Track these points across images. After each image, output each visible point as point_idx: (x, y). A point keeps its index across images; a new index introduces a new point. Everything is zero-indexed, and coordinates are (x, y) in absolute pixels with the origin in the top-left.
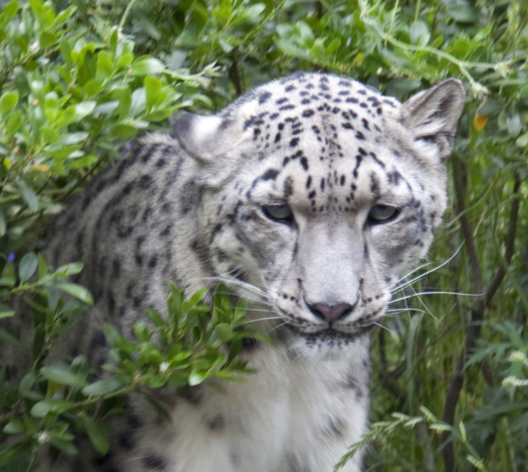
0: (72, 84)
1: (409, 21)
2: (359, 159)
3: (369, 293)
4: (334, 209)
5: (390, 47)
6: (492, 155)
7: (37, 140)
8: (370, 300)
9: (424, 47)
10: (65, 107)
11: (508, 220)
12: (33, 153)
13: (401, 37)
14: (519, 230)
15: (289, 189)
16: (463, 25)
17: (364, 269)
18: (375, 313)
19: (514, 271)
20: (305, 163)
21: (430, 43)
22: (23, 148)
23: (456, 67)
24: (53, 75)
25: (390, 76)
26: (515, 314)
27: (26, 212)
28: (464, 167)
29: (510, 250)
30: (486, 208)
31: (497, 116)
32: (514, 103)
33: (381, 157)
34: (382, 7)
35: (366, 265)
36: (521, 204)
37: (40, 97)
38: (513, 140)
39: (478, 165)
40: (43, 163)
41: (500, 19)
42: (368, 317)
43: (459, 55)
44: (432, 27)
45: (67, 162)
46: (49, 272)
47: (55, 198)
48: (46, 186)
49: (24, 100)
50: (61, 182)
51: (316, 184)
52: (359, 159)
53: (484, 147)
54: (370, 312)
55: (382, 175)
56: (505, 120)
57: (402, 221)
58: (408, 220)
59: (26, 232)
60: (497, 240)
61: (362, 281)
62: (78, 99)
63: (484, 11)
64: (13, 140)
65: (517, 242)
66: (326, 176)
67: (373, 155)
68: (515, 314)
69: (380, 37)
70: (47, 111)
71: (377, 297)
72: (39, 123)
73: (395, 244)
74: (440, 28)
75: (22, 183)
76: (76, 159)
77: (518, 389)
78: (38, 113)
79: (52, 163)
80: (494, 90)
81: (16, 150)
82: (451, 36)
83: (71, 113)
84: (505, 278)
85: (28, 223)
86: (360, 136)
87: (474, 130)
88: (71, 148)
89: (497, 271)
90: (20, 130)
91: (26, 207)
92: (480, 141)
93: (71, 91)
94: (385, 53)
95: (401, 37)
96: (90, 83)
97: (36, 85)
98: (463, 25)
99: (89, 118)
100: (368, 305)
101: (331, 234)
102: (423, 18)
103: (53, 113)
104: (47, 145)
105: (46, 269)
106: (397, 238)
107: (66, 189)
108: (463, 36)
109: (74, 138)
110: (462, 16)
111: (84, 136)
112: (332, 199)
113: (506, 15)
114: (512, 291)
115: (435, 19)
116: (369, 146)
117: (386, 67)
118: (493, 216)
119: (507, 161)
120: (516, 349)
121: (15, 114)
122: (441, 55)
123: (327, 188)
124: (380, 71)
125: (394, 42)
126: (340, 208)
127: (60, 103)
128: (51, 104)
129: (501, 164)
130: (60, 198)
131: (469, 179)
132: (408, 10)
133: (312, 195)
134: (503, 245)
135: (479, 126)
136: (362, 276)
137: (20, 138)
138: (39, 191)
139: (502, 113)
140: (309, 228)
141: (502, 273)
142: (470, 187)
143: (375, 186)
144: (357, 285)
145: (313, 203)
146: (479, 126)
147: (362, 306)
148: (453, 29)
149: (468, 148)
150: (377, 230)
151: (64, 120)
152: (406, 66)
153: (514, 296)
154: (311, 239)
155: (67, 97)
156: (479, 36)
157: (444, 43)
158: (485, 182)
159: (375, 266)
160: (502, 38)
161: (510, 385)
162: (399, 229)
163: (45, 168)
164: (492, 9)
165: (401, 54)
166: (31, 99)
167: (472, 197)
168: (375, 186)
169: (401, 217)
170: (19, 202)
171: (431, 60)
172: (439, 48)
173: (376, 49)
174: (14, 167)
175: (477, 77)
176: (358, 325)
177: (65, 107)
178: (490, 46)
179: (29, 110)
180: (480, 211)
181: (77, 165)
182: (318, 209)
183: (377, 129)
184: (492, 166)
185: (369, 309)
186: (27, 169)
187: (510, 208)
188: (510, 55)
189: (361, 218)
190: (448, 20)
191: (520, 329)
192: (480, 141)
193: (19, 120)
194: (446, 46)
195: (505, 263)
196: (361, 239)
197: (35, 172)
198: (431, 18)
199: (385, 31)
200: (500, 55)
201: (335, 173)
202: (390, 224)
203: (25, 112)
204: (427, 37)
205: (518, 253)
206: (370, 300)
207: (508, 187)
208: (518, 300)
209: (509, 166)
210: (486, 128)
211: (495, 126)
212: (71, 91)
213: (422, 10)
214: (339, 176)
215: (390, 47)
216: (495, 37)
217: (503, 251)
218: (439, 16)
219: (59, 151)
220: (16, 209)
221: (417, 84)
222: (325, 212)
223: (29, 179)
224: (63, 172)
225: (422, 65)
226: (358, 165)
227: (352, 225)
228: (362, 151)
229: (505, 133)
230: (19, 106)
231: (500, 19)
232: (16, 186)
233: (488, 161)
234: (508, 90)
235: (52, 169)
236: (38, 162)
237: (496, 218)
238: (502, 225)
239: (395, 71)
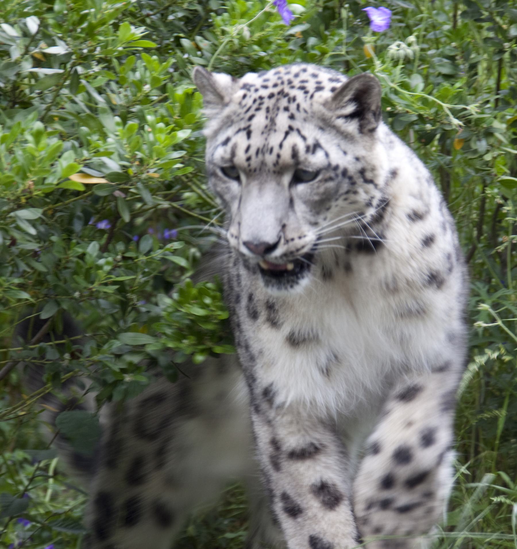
0: (176, 117)
1: (409, 75)
2: (287, 134)
3: (290, 234)
4: (265, 171)
5: (396, 92)
6: (466, 167)
7: (151, 157)
8: (293, 240)
9: (419, 93)
10: (170, 133)
11: (478, 212)
12: (148, 165)
13: (404, 85)
14: (486, 219)
15: (233, 154)
16: (447, 77)
17: (287, 216)
18: (298, 250)
19: (482, 247)
20: (249, 134)
21: (423, 91)
22: (141, 161)
23: (441, 106)
24: (162, 111)
25: (396, 112)
26: (483, 278)
27: (146, 207)
28: (448, 175)
29: (480, 233)
30: (463, 203)
31: (470, 140)
32: (483, 130)
33: (305, 132)
34: (391, 64)
35: (291, 213)
36: (488, 201)
37: (153, 126)
38: (481, 156)
39: (457, 174)
40: (155, 172)
41: (473, 72)
42: (292, 253)
43: (442, 98)
44: (426, 78)
45: (172, 171)
46: (161, 248)
47: (166, 197)
48: (159, 189)
49: (142, 128)
50: (169, 186)
51: (253, 151)
52: (287, 134)
53: (462, 161)
54: (293, 249)
55: (301, 146)
56: (475, 143)
57: (320, 181)
58: (326, 180)
59: (146, 220)
60: (471, 225)
61: (284, 226)
62: (180, 127)
63: (462, 67)
64: (134, 156)
65: (485, 227)
66: (261, 147)
67: (299, 131)
68: (483, 278)
69: (389, 85)
70: (158, 135)
71: (300, 238)
72: (152, 144)
73: (316, 198)
74: (432, 79)
75: (140, 185)
76: (179, 169)
77: (486, 329)
78: (151, 137)
79: (162, 172)
80: (468, 122)
81: (137, 163)
82: (438, 84)
83: (174, 137)
84: (476, 252)
85: (147, 215)
86: (292, 117)
87: (455, 150)
88: (174, 161)
89: (470, 247)
90: (139, 150)
91: (145, 204)
92: (459, 157)
93: (175, 123)
94: (393, 97)
95: (404, 85)
96: (188, 116)
97: (150, 118)
98: (447, 77)
99: (186, 141)
100: (291, 244)
101: (260, 190)
102: (419, 73)
103: (162, 137)
104: (158, 160)
105: (157, 247)
106: (317, 194)
107: (173, 191)
108: (446, 85)
109: (176, 155)
110: (446, 70)
111: (183, 153)
112: (263, 163)
113: (477, 70)
114: (480, 261)
115: (428, 72)
116: (296, 124)
117: (392, 105)
118: (467, 209)
119: (477, 171)
120: (483, 302)
121: (135, 137)
122: (431, 98)
123: (260, 156)
124: (389, 109)
125: (399, 89)
126: (269, 171)
127: (167, 130)
128: (161, 131)
129: (473, 173)
130: (169, 197)
131: (452, 184)
132: (409, 66)
133: (249, 159)
134: (475, 229)
135: (458, 147)
136: (285, 221)
137: (140, 155)
138: (153, 192)
139: (474, 138)
140: (248, 184)
141: (475, 248)
142: (452, 189)
143: (295, 154)
144: (279, 228)
145: (249, 165)
146: (458, 147)
147: (285, 244)
148: (440, 80)
149: (451, 162)
150: (301, 188)
151: (170, 142)
152: (407, 106)
153: (483, 264)
154: (249, 192)
155: (172, 126)
156: (458, 85)
157: (433, 89)
158: (462, 185)
159: (299, 214)
160: (474, 85)
161: (480, 327)
162: (318, 187)
163: (156, 175)
164: (467, 65)
165: (403, 98)
166: (147, 128)
167: (454, 196)
168: (295, 154)
169: (320, 177)
170: (140, 200)
171: (425, 102)
172: (430, 94)
173: (386, 95)
174: (136, 175)
175: (455, 113)
176: (285, 258)
177: (170, 133)
178: (465, 91)
179: (145, 135)
180: (459, 205)
181: (179, 174)
182: (253, 170)
183: (306, 111)
184: (467, 174)
185: (292, 246)
186: (144, 176)
187: (480, 203)
188: (479, 98)
189: (287, 179)
190: (437, 73)
191: (487, 287)
192: (459, 157)
193: (138, 142)
194: (435, 92)
195: (476, 241)
196: (287, 194)
197: (151, 178)
198: (425, 72)
199: (393, 81)
200: (473, 97)
201: (268, 144)
202: (311, 183)
203: (142, 136)
204: (421, 86)
205: (486, 235)
206: (293, 240)
207: (478, 189)
208: (485, 267)
209: (478, 175)
210: (463, 149)
211: (469, 147)
212: (175, 123)
213: (419, 66)
214: (270, 146)
215: (396, 92)
216: (469, 85)
217: (475, 233)
218: (431, 71)
219: (166, 164)
220: (139, 205)
221: (415, 118)
222: (258, 172)
223: (146, 183)
224: (169, 178)
225: (418, 105)
226: (285, 138)
227: (279, 183)
228: (291, 128)
229: (475, 151)
230: (138, 133)
231: (473, 72)
232: (137, 188)
233: (465, 171)
234: (479, 122)
235: (162, 177)
236: (152, 171)
237: (470, 211)
238: (474, 216)
239: (400, 109)
